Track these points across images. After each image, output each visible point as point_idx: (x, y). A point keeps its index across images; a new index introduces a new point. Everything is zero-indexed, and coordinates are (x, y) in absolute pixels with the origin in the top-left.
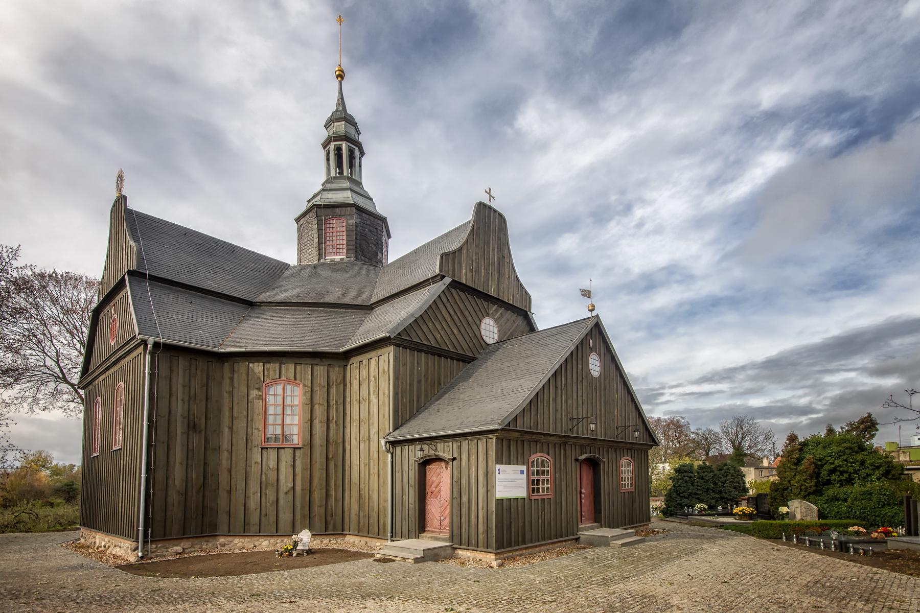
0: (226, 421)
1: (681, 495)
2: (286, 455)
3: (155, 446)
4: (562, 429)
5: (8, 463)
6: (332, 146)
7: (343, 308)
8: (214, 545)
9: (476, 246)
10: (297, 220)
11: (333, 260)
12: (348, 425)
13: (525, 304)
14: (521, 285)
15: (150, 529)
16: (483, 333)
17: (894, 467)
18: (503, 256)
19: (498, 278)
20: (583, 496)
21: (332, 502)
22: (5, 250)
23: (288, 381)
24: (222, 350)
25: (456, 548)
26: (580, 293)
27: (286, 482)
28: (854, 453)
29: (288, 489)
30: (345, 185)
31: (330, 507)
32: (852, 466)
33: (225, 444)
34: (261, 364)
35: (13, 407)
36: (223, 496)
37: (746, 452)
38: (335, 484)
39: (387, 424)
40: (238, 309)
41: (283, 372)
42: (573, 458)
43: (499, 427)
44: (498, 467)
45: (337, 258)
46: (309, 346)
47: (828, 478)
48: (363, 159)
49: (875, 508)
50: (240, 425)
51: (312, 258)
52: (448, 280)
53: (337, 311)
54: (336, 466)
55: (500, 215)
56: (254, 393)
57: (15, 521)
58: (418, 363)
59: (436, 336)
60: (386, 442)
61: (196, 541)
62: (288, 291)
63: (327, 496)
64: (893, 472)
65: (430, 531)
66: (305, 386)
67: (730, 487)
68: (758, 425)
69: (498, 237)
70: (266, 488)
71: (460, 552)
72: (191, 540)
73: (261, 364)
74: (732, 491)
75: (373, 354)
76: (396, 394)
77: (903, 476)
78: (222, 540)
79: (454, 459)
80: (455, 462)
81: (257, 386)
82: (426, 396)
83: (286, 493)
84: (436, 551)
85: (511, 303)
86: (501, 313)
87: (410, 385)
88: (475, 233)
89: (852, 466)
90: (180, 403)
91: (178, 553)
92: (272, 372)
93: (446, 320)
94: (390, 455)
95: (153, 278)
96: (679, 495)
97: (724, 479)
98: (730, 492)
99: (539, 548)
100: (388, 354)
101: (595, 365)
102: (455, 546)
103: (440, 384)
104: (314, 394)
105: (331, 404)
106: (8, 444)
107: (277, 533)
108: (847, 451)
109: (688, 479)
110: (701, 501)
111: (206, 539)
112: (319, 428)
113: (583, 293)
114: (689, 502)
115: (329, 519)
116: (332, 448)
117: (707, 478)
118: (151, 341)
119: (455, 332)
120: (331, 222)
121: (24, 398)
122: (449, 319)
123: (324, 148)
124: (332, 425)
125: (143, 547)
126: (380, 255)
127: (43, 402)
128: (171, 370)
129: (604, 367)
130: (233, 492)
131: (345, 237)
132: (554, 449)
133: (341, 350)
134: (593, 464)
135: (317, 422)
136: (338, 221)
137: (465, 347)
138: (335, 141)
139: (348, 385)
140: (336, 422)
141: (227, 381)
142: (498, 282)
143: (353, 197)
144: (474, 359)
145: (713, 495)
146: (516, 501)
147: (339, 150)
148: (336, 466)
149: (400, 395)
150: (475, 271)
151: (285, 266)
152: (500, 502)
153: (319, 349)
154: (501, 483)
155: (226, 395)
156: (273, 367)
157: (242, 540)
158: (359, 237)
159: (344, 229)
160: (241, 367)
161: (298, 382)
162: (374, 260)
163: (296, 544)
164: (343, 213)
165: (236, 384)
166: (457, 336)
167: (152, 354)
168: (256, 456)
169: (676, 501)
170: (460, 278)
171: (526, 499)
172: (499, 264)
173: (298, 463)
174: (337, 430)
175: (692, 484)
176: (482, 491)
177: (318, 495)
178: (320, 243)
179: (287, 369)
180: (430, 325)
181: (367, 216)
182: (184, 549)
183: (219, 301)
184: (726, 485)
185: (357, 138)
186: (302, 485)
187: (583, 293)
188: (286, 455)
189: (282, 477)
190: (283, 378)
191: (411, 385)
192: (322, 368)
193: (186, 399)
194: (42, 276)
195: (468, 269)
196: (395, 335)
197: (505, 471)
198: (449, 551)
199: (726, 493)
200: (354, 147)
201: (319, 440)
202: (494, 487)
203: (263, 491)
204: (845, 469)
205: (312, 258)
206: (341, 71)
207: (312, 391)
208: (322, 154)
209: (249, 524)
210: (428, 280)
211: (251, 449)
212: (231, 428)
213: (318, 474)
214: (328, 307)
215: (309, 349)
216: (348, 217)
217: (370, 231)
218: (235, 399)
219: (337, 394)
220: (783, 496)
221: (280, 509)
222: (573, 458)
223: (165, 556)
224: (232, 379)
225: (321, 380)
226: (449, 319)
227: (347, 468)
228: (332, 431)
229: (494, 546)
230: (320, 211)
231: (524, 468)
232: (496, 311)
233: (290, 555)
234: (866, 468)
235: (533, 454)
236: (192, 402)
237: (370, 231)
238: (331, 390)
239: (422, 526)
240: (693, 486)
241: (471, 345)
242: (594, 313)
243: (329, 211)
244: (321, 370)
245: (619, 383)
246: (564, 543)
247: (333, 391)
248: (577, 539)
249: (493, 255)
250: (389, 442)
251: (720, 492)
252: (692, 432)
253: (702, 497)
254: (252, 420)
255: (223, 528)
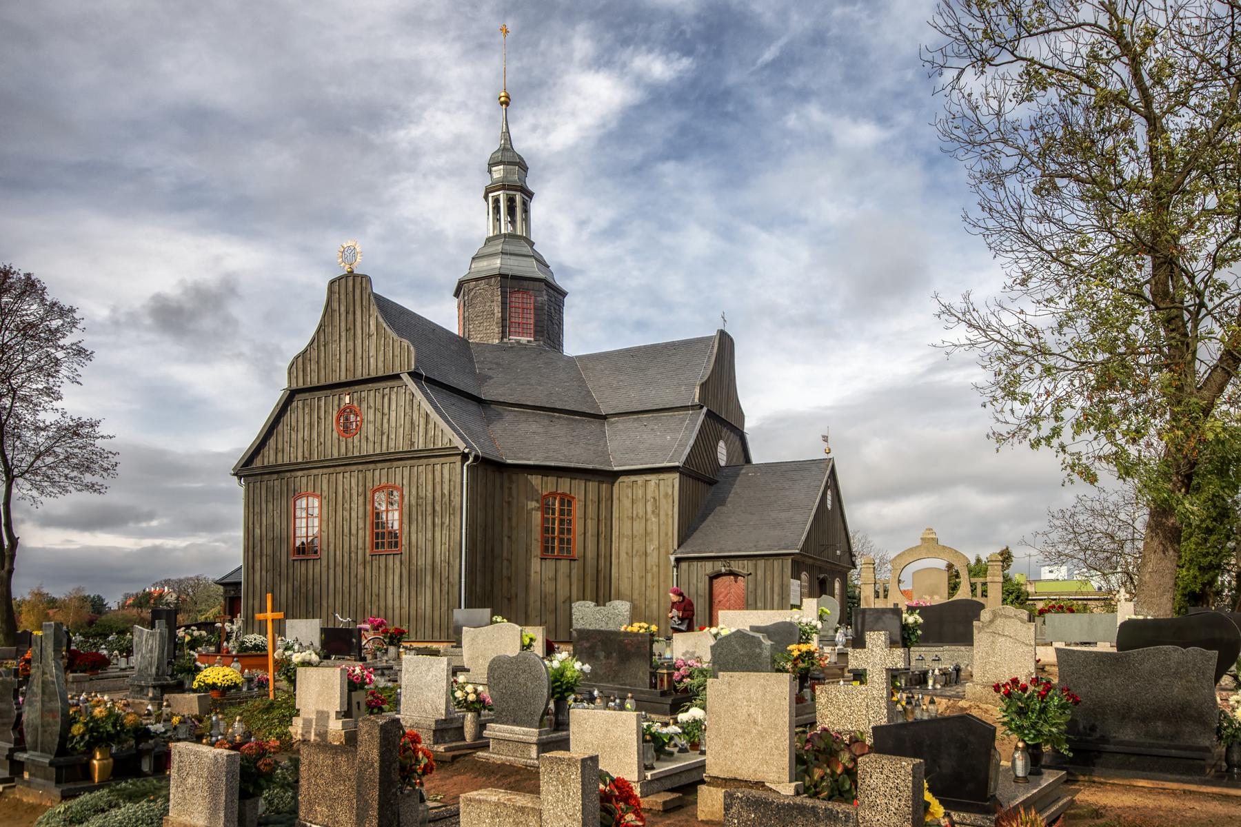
11: (518, 342)
17: (1022, 593)
26: (821, 438)
37: (856, 582)
45: (524, 340)
53: (573, 419)
64: (1022, 598)
68: (871, 544)
77: (1028, 602)
80: (750, 577)
83: (564, 602)
120: (517, 295)
131: (532, 316)
160: (522, 477)
165: (514, 493)
178: (503, 319)
216: (537, 293)
224: (510, 489)
242: (830, 456)
243: (515, 282)
247: (603, 505)
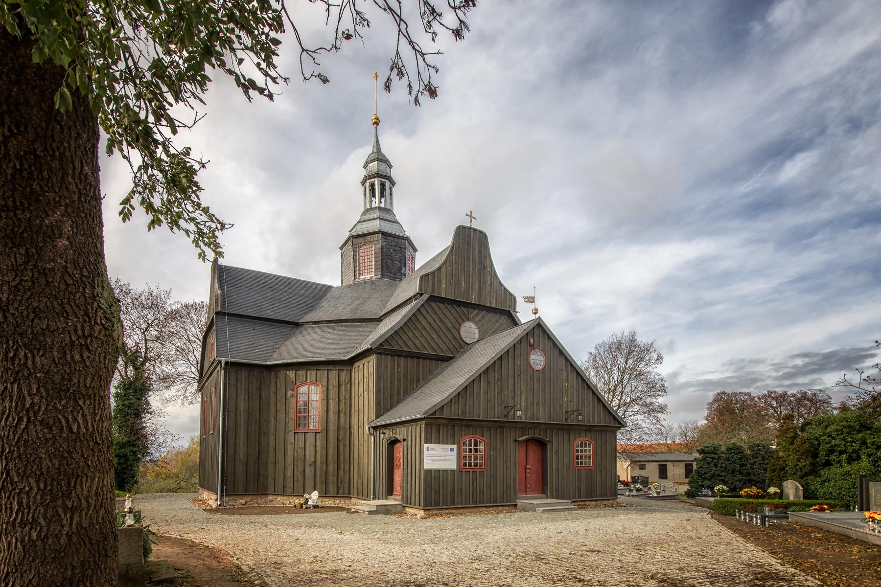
0: (272, 413)
1: (703, 476)
2: (310, 438)
3: (227, 431)
4: (496, 414)
5: (169, 443)
6: (368, 184)
7: (360, 322)
8: (265, 501)
9: (455, 263)
10: (341, 248)
11: (364, 279)
12: (353, 414)
13: (510, 304)
14: (505, 289)
15: (225, 487)
16: (462, 334)
18: (484, 266)
19: (479, 286)
20: (528, 471)
21: (341, 472)
22: (162, 293)
23: (311, 383)
24: (269, 363)
25: (405, 507)
27: (310, 457)
28: (855, 432)
29: (311, 462)
30: (375, 215)
31: (340, 477)
32: (852, 446)
33: (272, 430)
34: (294, 371)
35: (172, 403)
36: (271, 466)
38: (344, 459)
39: (373, 416)
40: (285, 329)
41: (309, 377)
42: (512, 439)
43: (423, 416)
44: (426, 446)
45: (368, 277)
46: (325, 356)
47: (827, 458)
48: (394, 189)
49: (850, 488)
50: (281, 415)
51: (350, 280)
52: (426, 297)
54: (344, 445)
55: (481, 232)
56: (290, 393)
57: (177, 488)
58: (398, 365)
59: (416, 342)
60: (369, 428)
61: (254, 497)
62: (324, 311)
63: (338, 468)
65: (396, 495)
66: (323, 386)
67: (759, 469)
69: (479, 251)
70: (297, 462)
71: (407, 509)
72: (251, 496)
73: (294, 371)
74: (761, 473)
75: (365, 361)
76: (378, 391)
78: (270, 497)
79: (404, 440)
81: (291, 387)
82: (405, 390)
83: (310, 465)
84: (389, 507)
85: (494, 306)
86: (483, 316)
87: (391, 383)
88: (454, 252)
89: (852, 446)
90: (243, 402)
91: (242, 505)
92: (301, 377)
93: (425, 329)
94: (373, 437)
95: (230, 315)
96: (700, 476)
97: (752, 461)
98: (759, 474)
99: (472, 510)
100: (373, 359)
101: (537, 360)
102: (405, 505)
103: (419, 380)
104: (329, 392)
105: (341, 399)
106: (165, 430)
107: (293, 494)
108: (845, 430)
109: (710, 460)
110: (725, 483)
111: (260, 496)
112: (332, 417)
113: (527, 300)
114: (711, 483)
115: (340, 485)
116: (342, 433)
117: (734, 460)
118: (223, 360)
119: (434, 337)
121: (178, 397)
122: (428, 328)
123: (363, 185)
124: (342, 415)
125: (221, 499)
126: (403, 269)
127: (190, 398)
128: (237, 379)
129: (549, 361)
130: (277, 464)
132: (489, 433)
133: (346, 358)
134: (542, 444)
135: (331, 413)
136: (368, 246)
137: (444, 348)
138: (369, 179)
139: (353, 384)
140: (344, 413)
141: (273, 385)
142: (480, 289)
143: (381, 224)
144: (452, 358)
145: (740, 477)
146: (445, 472)
147: (372, 186)
148: (344, 445)
149: (382, 391)
150: (455, 284)
151: (328, 289)
152: (429, 472)
153: (331, 358)
154: (428, 458)
155: (272, 395)
156: (301, 373)
157: (283, 498)
158: (384, 258)
159: (373, 252)
160: (282, 374)
161: (318, 383)
162: (399, 274)
163: (307, 501)
164: (372, 240)
165: (278, 387)
166: (436, 340)
167: (225, 369)
168: (291, 438)
169: (698, 482)
170: (440, 293)
171: (456, 472)
172: (480, 274)
173: (318, 443)
174: (345, 419)
175: (716, 466)
176: (418, 463)
177: (332, 468)
179: (311, 374)
180: (410, 334)
181: (392, 239)
182: (246, 502)
183: (274, 325)
184: (755, 466)
185: (388, 171)
186: (321, 460)
187: (527, 300)
188: (310, 438)
189: (307, 454)
190: (308, 381)
191: (392, 383)
192: (335, 372)
193: (247, 398)
194: (186, 306)
195: (448, 283)
196: (376, 346)
197: (433, 449)
198: (400, 508)
199: (754, 475)
200: (385, 180)
201: (332, 427)
202: (423, 461)
203: (295, 463)
204: (844, 448)
205: (350, 280)
206: (377, 119)
207: (327, 389)
208: (362, 188)
209: (286, 487)
210: (411, 298)
211: (288, 433)
212: (276, 419)
213: (331, 451)
214: (349, 322)
215: (324, 359)
217: (394, 250)
218: (278, 397)
219: (345, 392)
220: (779, 477)
221: (306, 477)
222: (512, 439)
223: (234, 506)
224: (276, 383)
225: (334, 381)
226: (428, 328)
227: (352, 447)
228: (342, 420)
229: (422, 505)
230: (357, 241)
231: (455, 447)
232: (477, 314)
233: (302, 507)
234: (867, 447)
235: (465, 436)
236: (250, 401)
237: (394, 250)
238: (341, 388)
239: (390, 491)
240: (716, 468)
241: (450, 346)
242: (537, 316)
243: (361, 239)
244: (334, 374)
245: (569, 372)
246: (500, 508)
247: (342, 389)
248: (515, 505)
249: (474, 268)
250: (372, 427)
251: (749, 474)
252: (833, 408)
253: (726, 479)
254: (289, 412)
255: (271, 489)
